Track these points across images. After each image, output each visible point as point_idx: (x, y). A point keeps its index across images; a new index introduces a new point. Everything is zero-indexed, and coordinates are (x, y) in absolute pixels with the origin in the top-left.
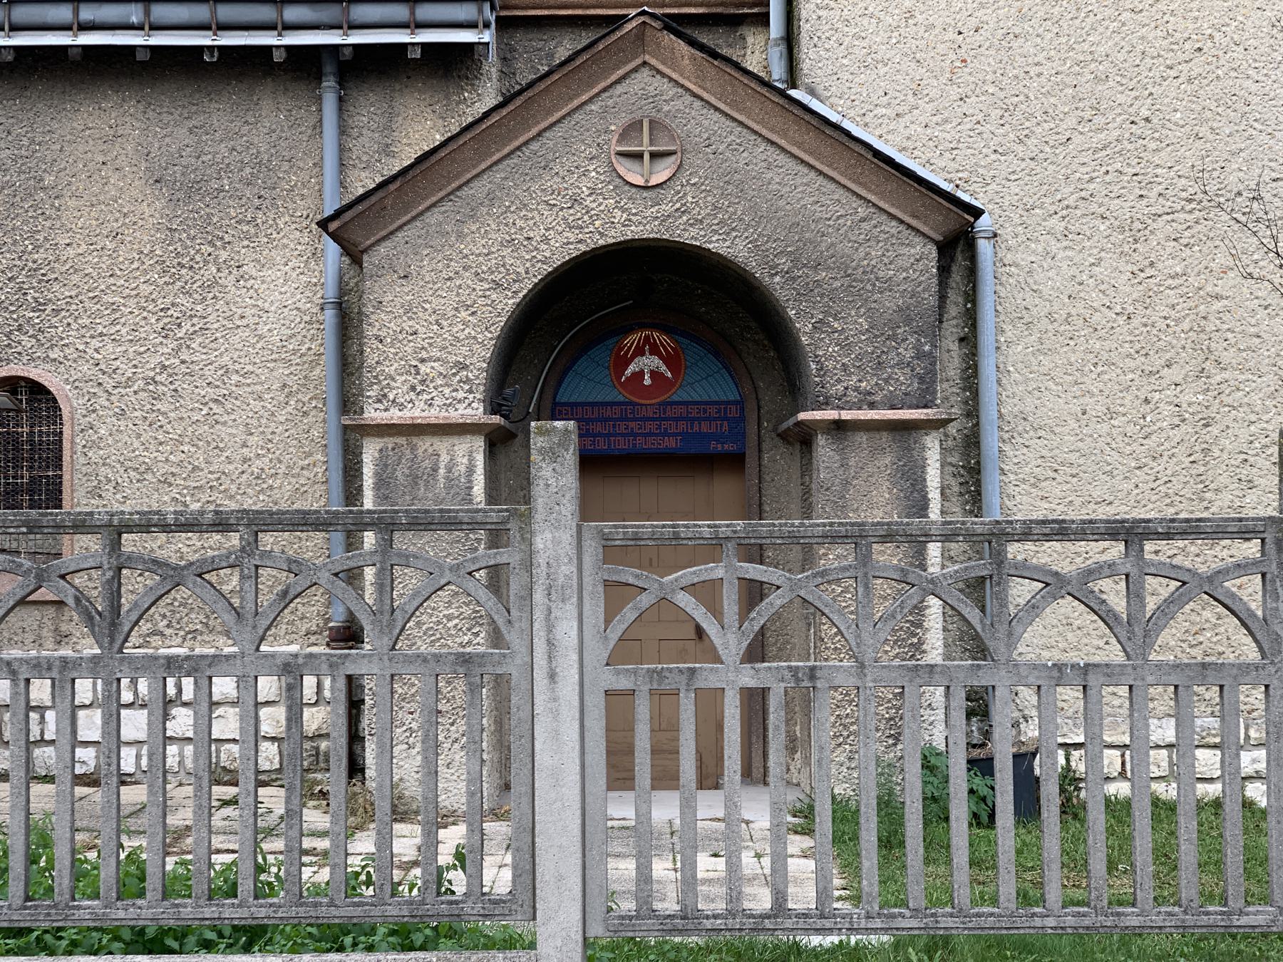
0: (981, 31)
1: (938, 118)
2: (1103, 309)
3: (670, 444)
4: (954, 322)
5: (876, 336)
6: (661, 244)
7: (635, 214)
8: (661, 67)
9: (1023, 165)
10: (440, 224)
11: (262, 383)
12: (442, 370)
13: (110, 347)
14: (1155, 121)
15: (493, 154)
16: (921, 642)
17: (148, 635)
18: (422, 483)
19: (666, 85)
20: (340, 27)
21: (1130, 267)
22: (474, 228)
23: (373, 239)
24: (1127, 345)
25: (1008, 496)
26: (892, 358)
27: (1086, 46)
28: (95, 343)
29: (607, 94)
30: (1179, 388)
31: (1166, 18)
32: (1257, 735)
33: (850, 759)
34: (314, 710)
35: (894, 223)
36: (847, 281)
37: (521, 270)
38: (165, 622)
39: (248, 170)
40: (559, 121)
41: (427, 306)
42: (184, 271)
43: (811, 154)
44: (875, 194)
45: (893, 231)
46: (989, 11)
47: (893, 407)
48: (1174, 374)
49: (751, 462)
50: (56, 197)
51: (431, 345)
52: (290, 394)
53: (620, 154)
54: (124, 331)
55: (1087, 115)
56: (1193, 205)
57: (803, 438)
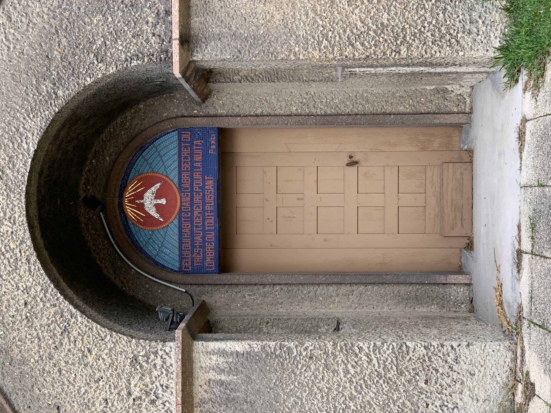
3: (211, 184)
5: (109, 8)
7: (5, 214)
10: (13, 379)
12: (137, 378)
18: (233, 395)
22: (17, 351)
33: (470, 33)
36: (62, 33)
37: (52, 310)
41: (83, 390)
49: (224, 123)
51: (116, 387)
57: (204, 78)
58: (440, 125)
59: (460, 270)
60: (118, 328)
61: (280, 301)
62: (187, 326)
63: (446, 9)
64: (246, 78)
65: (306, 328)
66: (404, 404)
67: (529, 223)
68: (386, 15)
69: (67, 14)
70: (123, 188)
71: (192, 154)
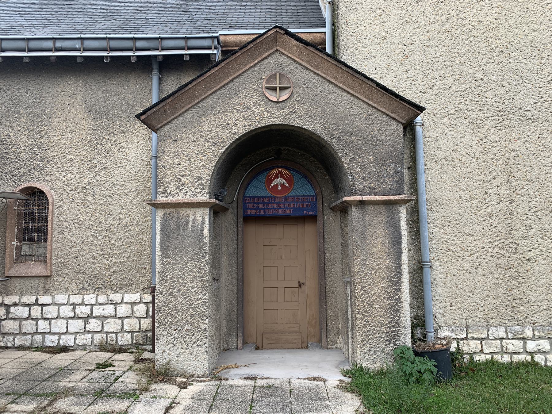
0: (413, 45)
1: (397, 79)
2: (467, 155)
3: (288, 212)
4: (406, 161)
6: (284, 127)
7: (273, 114)
8: (284, 52)
9: (432, 97)
11: (127, 189)
12: (191, 180)
13: (69, 175)
14: (485, 80)
15: (213, 88)
16: (400, 298)
17: (81, 289)
18: (181, 228)
19: (286, 59)
20: (158, 50)
21: (477, 139)
22: (205, 120)
23: (161, 124)
24: (477, 170)
25: (430, 233)
26: (385, 173)
27: (456, 51)
28: (63, 174)
29: (261, 63)
30: (499, 188)
31: (488, 39)
32: (538, 334)
33: (369, 351)
34: (146, 320)
35: (384, 116)
36: (364, 141)
37: (225, 137)
38: (87, 284)
39: (124, 107)
40: (241, 75)
42: (98, 146)
43: (348, 87)
44: (376, 103)
45: (384, 119)
46: (416, 37)
47: (385, 195)
48: (497, 182)
49: (319, 218)
50: (50, 118)
51: (186, 169)
52: (138, 193)
53: (267, 88)
54: (75, 169)
55: (457, 77)
56: (501, 114)
57: (344, 210)
58: (321, 332)
59: (245, 343)
60: (216, 170)
61: (229, 248)
62: (217, 204)
63: (381, 338)
64: (343, 231)
65: (215, 264)
66: (176, 318)
67: (271, 384)
68: (377, 306)
69: (374, 143)
70: (286, 168)
71: (303, 202)
